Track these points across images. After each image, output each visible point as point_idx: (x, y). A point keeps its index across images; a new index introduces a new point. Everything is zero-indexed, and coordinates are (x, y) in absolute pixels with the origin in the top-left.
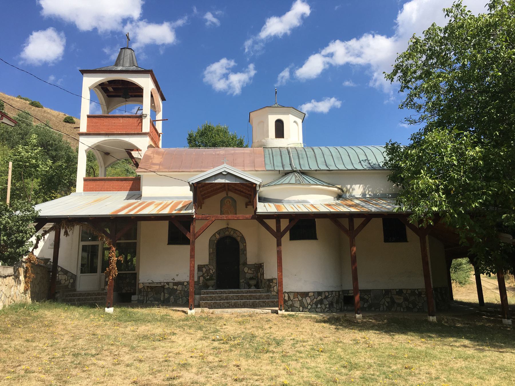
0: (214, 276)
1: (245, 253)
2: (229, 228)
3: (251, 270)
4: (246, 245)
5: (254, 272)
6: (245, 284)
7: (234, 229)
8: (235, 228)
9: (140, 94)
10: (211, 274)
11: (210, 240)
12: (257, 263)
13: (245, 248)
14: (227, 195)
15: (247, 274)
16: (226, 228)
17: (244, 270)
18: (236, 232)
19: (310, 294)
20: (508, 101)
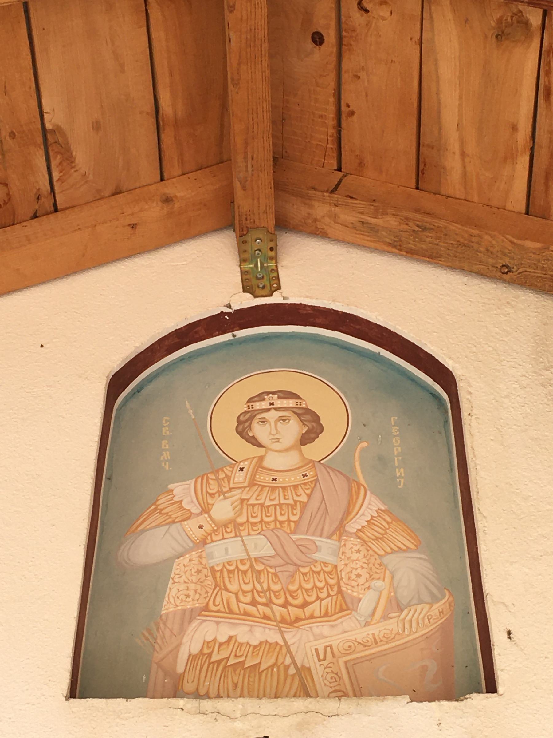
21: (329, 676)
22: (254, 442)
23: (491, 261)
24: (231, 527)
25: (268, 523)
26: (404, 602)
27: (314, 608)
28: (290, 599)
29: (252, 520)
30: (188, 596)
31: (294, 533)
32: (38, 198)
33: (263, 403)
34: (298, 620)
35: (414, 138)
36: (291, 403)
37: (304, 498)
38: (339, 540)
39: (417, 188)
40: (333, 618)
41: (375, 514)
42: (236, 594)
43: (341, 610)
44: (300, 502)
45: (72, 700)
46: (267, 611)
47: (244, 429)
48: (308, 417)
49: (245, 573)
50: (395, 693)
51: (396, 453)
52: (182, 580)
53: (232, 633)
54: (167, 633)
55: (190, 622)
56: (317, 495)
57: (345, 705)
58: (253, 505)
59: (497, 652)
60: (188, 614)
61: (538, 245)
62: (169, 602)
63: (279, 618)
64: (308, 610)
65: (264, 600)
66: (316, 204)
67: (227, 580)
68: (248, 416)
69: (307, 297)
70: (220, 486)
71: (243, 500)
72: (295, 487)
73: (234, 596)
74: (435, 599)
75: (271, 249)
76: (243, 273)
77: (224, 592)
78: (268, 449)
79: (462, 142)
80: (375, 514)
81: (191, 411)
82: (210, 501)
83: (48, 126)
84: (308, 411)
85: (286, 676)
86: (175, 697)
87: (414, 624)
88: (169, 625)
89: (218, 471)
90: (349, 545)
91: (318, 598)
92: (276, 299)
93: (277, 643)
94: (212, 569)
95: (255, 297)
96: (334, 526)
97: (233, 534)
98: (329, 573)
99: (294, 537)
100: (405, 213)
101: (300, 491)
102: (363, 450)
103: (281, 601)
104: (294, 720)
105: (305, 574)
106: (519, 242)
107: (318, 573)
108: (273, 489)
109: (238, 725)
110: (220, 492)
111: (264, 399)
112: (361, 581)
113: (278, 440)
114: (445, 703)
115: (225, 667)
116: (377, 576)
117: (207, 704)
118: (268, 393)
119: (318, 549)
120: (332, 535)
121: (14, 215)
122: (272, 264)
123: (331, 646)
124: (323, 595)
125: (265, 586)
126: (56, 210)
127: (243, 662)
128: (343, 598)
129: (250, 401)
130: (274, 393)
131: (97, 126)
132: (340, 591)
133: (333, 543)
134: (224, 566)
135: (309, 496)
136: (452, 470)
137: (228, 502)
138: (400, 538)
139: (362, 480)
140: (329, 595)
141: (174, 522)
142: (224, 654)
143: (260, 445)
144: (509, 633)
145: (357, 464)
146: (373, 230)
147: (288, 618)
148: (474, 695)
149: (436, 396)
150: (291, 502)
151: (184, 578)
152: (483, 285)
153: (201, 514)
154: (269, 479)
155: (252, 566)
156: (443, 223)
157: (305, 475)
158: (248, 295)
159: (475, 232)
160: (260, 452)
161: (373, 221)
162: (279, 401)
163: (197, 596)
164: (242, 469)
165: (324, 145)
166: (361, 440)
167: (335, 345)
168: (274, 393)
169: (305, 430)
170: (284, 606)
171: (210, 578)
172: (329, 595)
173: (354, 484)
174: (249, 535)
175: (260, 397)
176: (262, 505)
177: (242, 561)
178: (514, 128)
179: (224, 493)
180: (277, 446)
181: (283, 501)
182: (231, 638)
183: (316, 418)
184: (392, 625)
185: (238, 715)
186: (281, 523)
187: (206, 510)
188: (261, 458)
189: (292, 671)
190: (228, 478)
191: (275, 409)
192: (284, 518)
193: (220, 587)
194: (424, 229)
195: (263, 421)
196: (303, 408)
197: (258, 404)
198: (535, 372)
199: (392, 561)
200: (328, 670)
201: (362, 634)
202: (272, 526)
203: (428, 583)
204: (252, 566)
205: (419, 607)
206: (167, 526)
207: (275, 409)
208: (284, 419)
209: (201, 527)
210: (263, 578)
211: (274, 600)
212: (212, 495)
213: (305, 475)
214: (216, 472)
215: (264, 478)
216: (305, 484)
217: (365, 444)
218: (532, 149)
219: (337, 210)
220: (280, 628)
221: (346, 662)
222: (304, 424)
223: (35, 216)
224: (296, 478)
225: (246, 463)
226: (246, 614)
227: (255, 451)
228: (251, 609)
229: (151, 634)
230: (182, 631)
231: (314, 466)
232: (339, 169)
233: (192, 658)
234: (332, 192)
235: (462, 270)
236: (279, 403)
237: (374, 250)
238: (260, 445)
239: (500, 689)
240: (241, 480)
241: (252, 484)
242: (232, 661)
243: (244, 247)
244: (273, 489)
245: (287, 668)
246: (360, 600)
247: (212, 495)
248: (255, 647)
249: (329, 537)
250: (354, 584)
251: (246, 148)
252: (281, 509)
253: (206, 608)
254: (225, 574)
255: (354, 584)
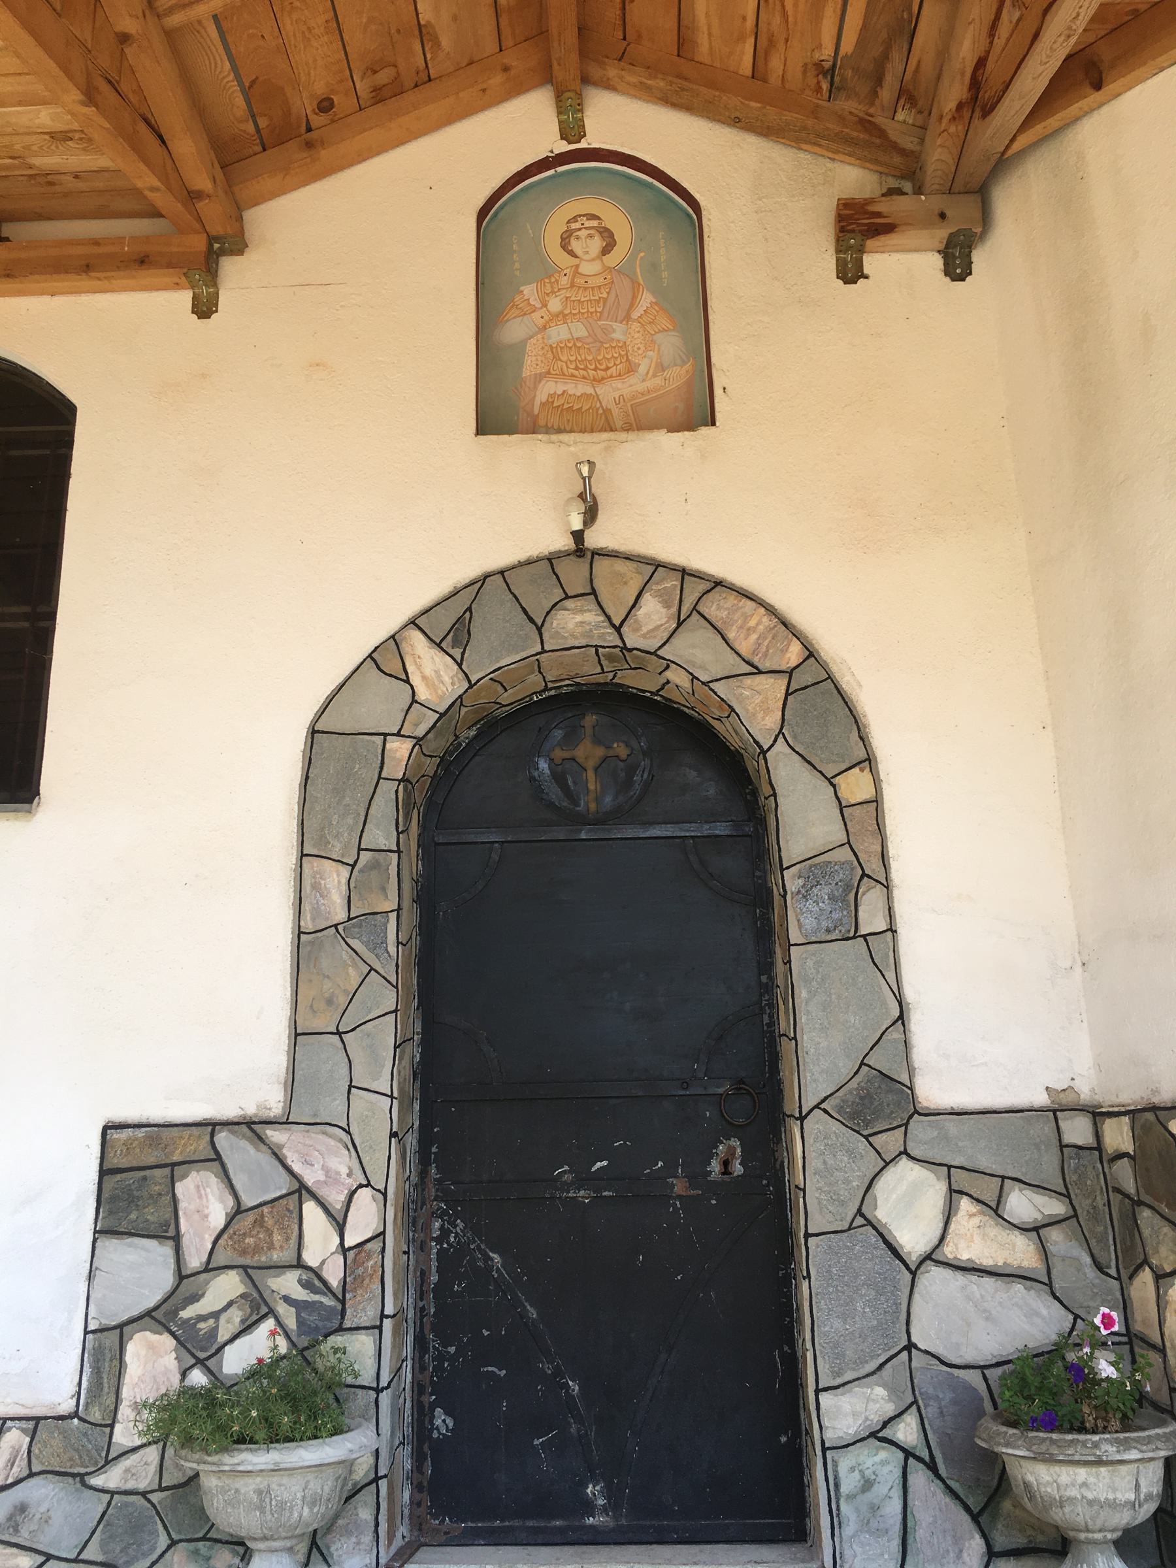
0: (362, 1311)
1: (872, 920)
2: (597, 553)
3: (995, 1209)
4: (876, 802)
5: (1056, 1237)
6: (920, 1478)
7: (684, 573)
8: (696, 562)
9: (60, 428)
10: (314, 1279)
11: (313, 732)
12: (1086, 1090)
13: (868, 847)
14: (571, 129)
15: (934, 1279)
16: (551, 560)
17: (883, 1213)
18: (715, 607)
19: (89, 1401)
20: (679, 1278)
21: (622, 414)
22: (572, 254)
23: (727, 113)
24: (561, 316)
25: (583, 313)
26: (665, 365)
27: (613, 371)
28: (598, 365)
29: (574, 312)
30: (537, 365)
31: (599, 319)
32: (418, 73)
33: (577, 224)
34: (603, 379)
35: (676, 20)
36: (595, 223)
37: (605, 295)
38: (627, 324)
39: (679, 56)
40: (624, 377)
41: (649, 306)
42: (566, 363)
43: (629, 372)
44: (603, 298)
45: (479, 436)
46: (585, 373)
47: (565, 244)
48: (606, 234)
49: (571, 348)
50: (658, 428)
51: (662, 260)
52: (533, 354)
53: (565, 389)
54: (527, 389)
55: (540, 381)
56: (613, 295)
57: (631, 436)
58: (574, 301)
59: (716, 401)
60: (538, 376)
61: (759, 105)
62: (526, 369)
63: (592, 378)
64: (609, 372)
65: (582, 367)
66: (608, 68)
67: (560, 353)
68: (568, 234)
69: (604, 143)
70: (552, 287)
71: (567, 298)
72: (599, 287)
73: (564, 364)
74: (684, 363)
75: (579, 105)
76: (560, 122)
77: (559, 362)
78: (582, 259)
79: (709, 28)
80: (649, 306)
81: (530, 231)
82: (547, 298)
83: (422, 22)
84: (607, 230)
85: (597, 415)
86: (534, 433)
87: (671, 380)
88: (528, 383)
89: (550, 276)
90: (633, 327)
91: (615, 364)
92: (583, 144)
93: (591, 394)
94: (551, 346)
95: (569, 143)
96: (624, 314)
97: (562, 322)
98: (621, 347)
99: (600, 323)
100: (670, 78)
101: (603, 290)
102: (641, 258)
103: (593, 367)
104: (602, 445)
105: (606, 348)
106: (747, 102)
107: (615, 347)
108: (586, 289)
109: (572, 449)
110: (553, 292)
111: (577, 221)
112: (640, 352)
113: (587, 252)
114: (686, 433)
115: (562, 410)
116: (650, 349)
117: (554, 437)
118: (580, 216)
119: (614, 331)
120: (623, 321)
121: (402, 86)
122: (579, 115)
123: (623, 395)
124: (618, 362)
125: (583, 358)
126: (430, 80)
127: (572, 406)
128: (630, 364)
129: (568, 222)
130: (584, 216)
131: (455, 18)
132: (628, 359)
133: (623, 326)
134: (558, 344)
135: (608, 293)
136: (697, 272)
137: (558, 298)
138: (664, 322)
139: (641, 282)
140: (621, 362)
141: (525, 314)
142: (561, 401)
143: (576, 257)
144: (724, 389)
145: (638, 270)
146: (648, 88)
147: (597, 377)
148: (703, 428)
149: (689, 216)
150: (597, 298)
151: (534, 353)
152: (722, 130)
153: (541, 308)
154: (583, 282)
155: (575, 344)
156: (695, 87)
157: (605, 279)
158: (564, 142)
159: (717, 93)
160: (576, 261)
161: (649, 82)
162: (587, 222)
163: (543, 365)
164: (565, 275)
165: (614, 21)
166: (640, 251)
167: (624, 176)
168: (584, 216)
169: (604, 244)
170: (595, 370)
171: (550, 353)
172: (621, 362)
173: (636, 285)
174: (572, 322)
175: (575, 219)
176: (579, 300)
177: (569, 341)
178: (744, 18)
179: (555, 292)
180: (586, 257)
181: (592, 298)
182: (564, 391)
183: (612, 235)
184: (658, 381)
185: (572, 443)
186: (592, 313)
187: (545, 305)
188: (577, 266)
189: (601, 411)
190: (557, 281)
191: (586, 228)
192: (593, 310)
193: (556, 358)
194: (683, 90)
195: (578, 238)
196: (603, 227)
197: (573, 224)
198: (752, 202)
199: (659, 338)
200: (621, 410)
201: (641, 387)
202: (586, 316)
203: (681, 354)
204: (575, 344)
205: (674, 369)
206: (521, 318)
207: (586, 228)
208: (591, 236)
209: (542, 317)
210: (582, 351)
211: (589, 366)
212: (548, 294)
213: (605, 279)
214: (550, 277)
215: (580, 281)
216: (606, 285)
217: (642, 254)
218: (756, 33)
219: (623, 73)
220: (593, 384)
221: (632, 405)
222: (604, 240)
223: (416, 86)
224: (599, 281)
225: (568, 270)
226: (573, 376)
227: (573, 261)
228: (576, 373)
229: (517, 390)
230: (535, 388)
231: (611, 271)
232: (624, 39)
233: (543, 404)
234: (620, 60)
235: (708, 118)
236: (588, 224)
237: (648, 101)
238: (576, 257)
239: (718, 424)
240: (566, 282)
241: (572, 285)
242: (566, 406)
243: (560, 104)
244: (586, 289)
245: (598, 409)
246: (639, 365)
247: (548, 294)
248: (579, 397)
249: (621, 323)
250: (636, 354)
251: (560, 36)
252: (591, 304)
253: (549, 373)
254: (559, 349)
255: (636, 354)
